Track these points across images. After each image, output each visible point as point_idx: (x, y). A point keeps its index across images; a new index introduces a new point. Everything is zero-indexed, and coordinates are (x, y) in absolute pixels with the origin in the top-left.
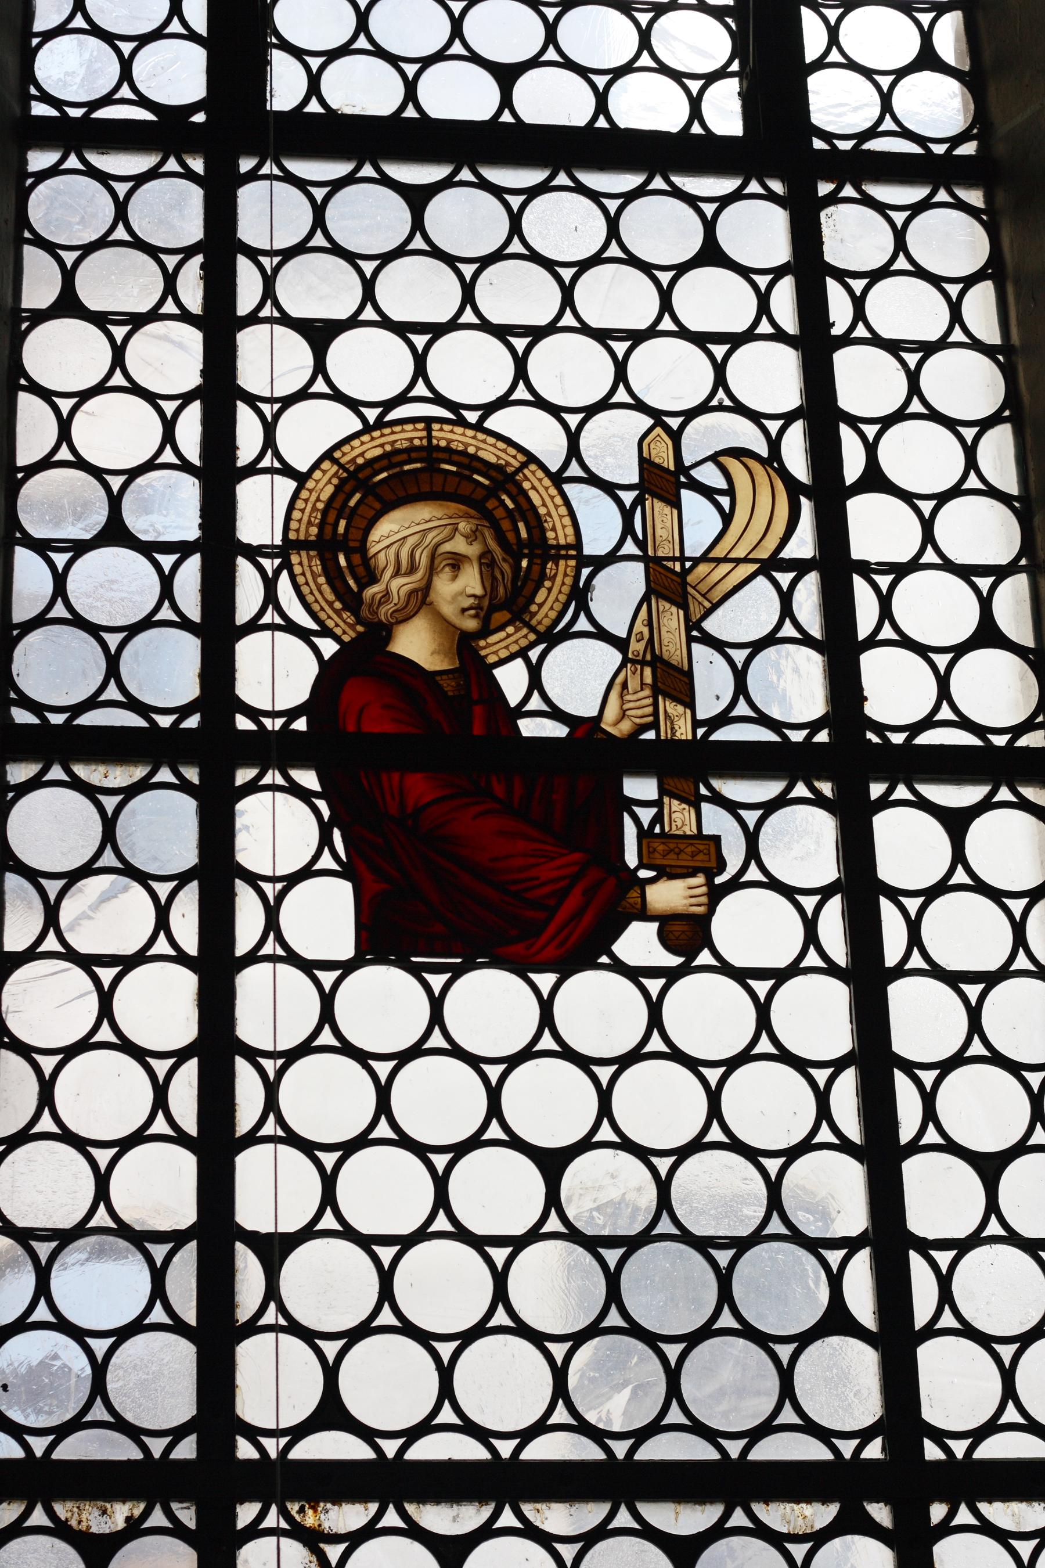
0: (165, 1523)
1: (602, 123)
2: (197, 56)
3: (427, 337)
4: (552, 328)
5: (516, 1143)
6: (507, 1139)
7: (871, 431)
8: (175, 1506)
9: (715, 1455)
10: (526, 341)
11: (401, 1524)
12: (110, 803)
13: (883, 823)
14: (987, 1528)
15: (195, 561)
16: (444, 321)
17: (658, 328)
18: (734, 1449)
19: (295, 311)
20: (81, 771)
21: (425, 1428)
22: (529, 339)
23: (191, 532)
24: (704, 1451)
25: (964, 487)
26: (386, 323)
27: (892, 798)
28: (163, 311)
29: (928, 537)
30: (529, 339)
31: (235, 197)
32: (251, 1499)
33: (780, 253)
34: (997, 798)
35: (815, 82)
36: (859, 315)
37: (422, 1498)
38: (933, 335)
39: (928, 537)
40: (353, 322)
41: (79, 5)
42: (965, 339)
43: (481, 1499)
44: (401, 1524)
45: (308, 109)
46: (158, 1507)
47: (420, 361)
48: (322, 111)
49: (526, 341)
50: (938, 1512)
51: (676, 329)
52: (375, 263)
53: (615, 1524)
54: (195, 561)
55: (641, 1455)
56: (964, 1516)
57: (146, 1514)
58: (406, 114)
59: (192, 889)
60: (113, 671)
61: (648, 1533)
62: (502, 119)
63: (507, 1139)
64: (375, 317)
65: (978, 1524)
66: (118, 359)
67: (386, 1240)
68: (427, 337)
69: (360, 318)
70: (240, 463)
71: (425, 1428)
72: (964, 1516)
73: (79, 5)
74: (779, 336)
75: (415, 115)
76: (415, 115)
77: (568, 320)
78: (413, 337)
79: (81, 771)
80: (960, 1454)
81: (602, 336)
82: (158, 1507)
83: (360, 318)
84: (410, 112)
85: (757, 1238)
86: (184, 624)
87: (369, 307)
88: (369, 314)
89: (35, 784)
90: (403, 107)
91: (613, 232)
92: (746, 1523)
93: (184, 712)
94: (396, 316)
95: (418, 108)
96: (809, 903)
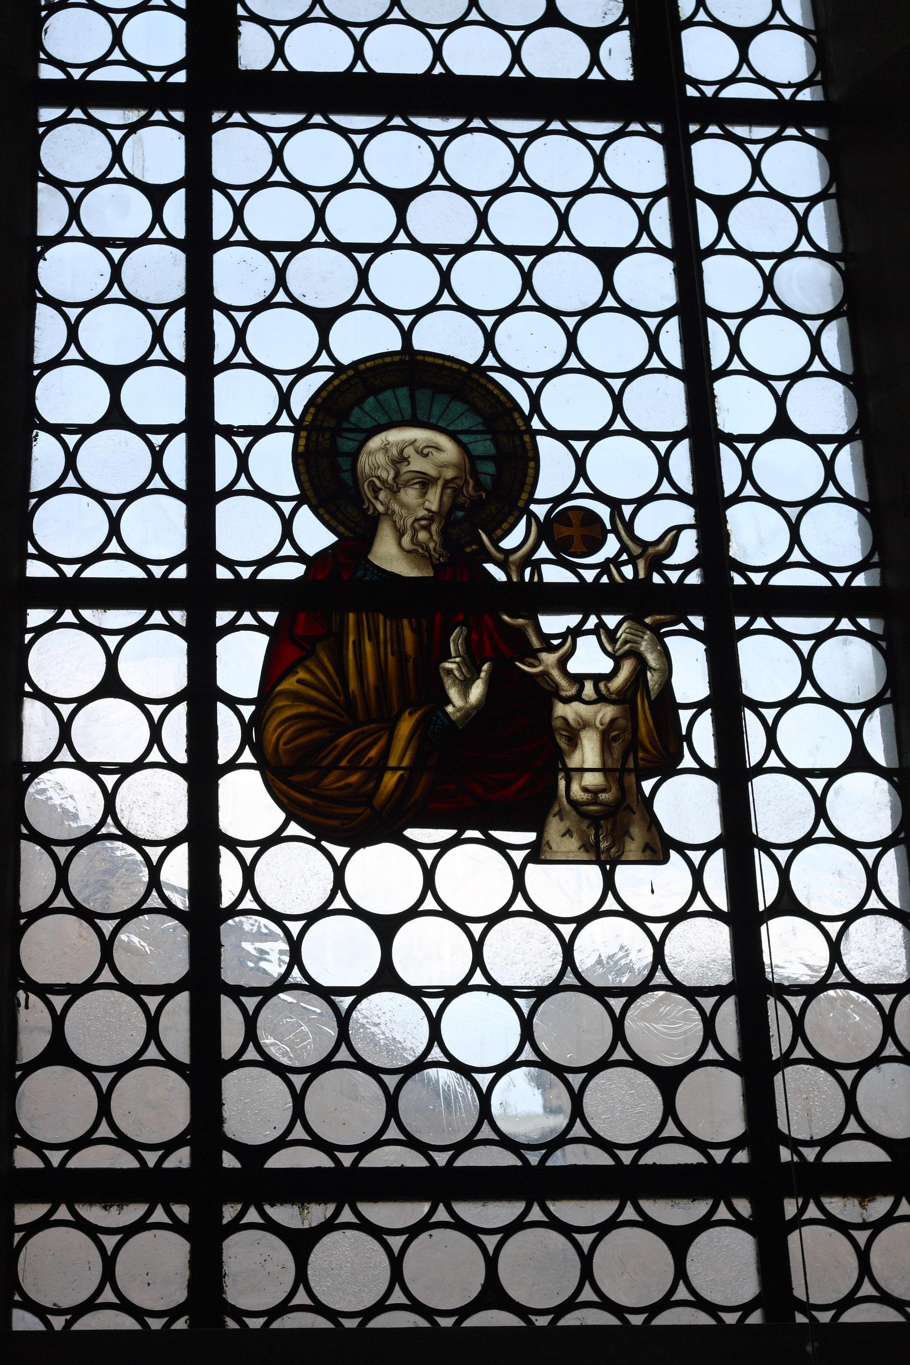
0: (543, 1218)
1: (359, 68)
2: (178, 26)
3: (286, 254)
4: (551, 248)
5: (357, 912)
6: (259, 909)
7: (733, 324)
8: (825, 1201)
9: (135, 1164)
10: (450, 257)
11: (167, 1220)
12: (112, 641)
13: (747, 648)
14: (460, 1225)
15: (181, 440)
16: (624, 246)
17: (395, 242)
18: (56, 1158)
19: (588, 241)
20: (87, 614)
21: (86, 1141)
22: (452, 256)
23: (178, 416)
24: (416, 1160)
25: (234, 361)
26: (497, 247)
27: (838, 628)
28: (396, 241)
29: (618, 408)
30: (452, 256)
31: (210, 141)
32: (235, 1201)
33: (657, 179)
34: (241, 622)
35: (689, 37)
36: (239, 220)
37: (90, 1200)
38: (462, 240)
39: (618, 408)
40: (632, 249)
41: (701, 1)
42: (810, 249)
43: (321, 1199)
44: (167, 1220)
45: (591, 77)
46: (629, 1204)
47: (363, 274)
48: (523, 76)
49: (450, 257)
50: (229, 1212)
51: (492, 243)
52: (244, 192)
53: (152, 1219)
54: (181, 440)
55: (72, 1164)
56: (812, 1212)
57: (337, 1213)
58: (356, 70)
59: (182, 709)
60: (114, 529)
61: (648, 1223)
62: (356, 70)
63: (259, 909)
64: (489, 242)
65: (171, 1222)
66: (445, 283)
67: (153, 990)
68: (286, 254)
69: (476, 243)
70: (714, 367)
71: (86, 1141)
72: (812, 1212)
73: (701, 1)
74: (170, 240)
75: (363, 70)
76: (363, 70)
77: (484, 239)
78: (520, 258)
79: (88, 614)
80: (55, 1163)
81: (511, 252)
82: (629, 1204)
83: (476, 243)
84: (280, 67)
85: (89, 986)
86: (172, 491)
87: (564, 235)
88: (484, 239)
89: (51, 626)
90: (273, 63)
91: (359, 162)
92: (818, 1215)
93: (173, 563)
94: (506, 241)
95: (366, 65)
96: (156, 711)
